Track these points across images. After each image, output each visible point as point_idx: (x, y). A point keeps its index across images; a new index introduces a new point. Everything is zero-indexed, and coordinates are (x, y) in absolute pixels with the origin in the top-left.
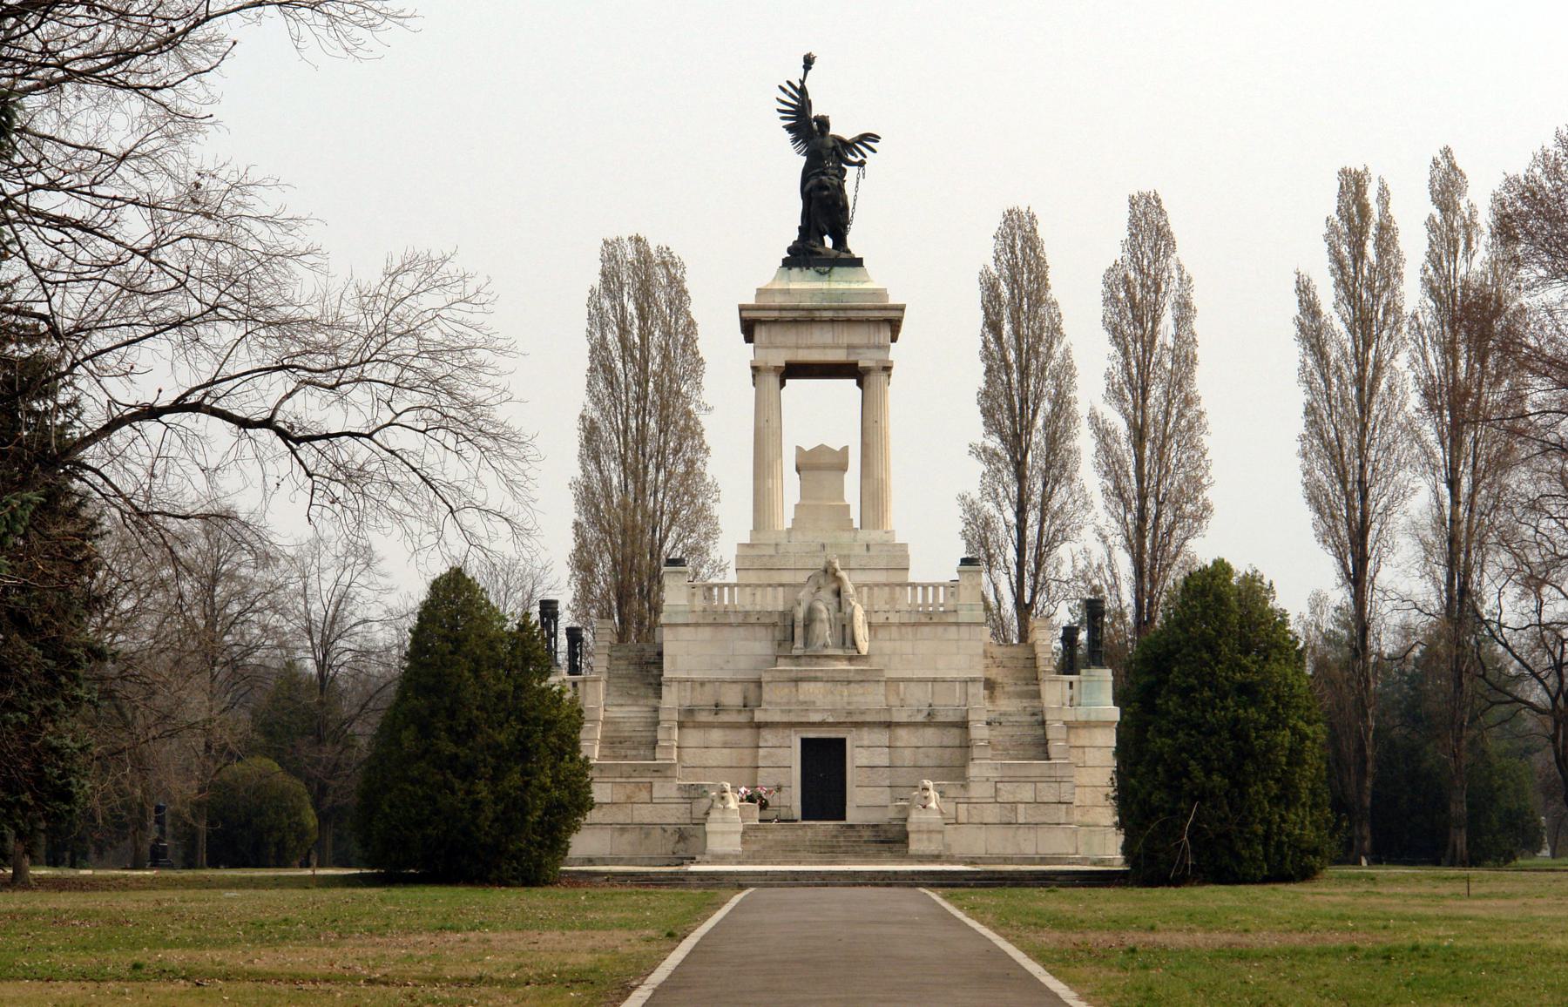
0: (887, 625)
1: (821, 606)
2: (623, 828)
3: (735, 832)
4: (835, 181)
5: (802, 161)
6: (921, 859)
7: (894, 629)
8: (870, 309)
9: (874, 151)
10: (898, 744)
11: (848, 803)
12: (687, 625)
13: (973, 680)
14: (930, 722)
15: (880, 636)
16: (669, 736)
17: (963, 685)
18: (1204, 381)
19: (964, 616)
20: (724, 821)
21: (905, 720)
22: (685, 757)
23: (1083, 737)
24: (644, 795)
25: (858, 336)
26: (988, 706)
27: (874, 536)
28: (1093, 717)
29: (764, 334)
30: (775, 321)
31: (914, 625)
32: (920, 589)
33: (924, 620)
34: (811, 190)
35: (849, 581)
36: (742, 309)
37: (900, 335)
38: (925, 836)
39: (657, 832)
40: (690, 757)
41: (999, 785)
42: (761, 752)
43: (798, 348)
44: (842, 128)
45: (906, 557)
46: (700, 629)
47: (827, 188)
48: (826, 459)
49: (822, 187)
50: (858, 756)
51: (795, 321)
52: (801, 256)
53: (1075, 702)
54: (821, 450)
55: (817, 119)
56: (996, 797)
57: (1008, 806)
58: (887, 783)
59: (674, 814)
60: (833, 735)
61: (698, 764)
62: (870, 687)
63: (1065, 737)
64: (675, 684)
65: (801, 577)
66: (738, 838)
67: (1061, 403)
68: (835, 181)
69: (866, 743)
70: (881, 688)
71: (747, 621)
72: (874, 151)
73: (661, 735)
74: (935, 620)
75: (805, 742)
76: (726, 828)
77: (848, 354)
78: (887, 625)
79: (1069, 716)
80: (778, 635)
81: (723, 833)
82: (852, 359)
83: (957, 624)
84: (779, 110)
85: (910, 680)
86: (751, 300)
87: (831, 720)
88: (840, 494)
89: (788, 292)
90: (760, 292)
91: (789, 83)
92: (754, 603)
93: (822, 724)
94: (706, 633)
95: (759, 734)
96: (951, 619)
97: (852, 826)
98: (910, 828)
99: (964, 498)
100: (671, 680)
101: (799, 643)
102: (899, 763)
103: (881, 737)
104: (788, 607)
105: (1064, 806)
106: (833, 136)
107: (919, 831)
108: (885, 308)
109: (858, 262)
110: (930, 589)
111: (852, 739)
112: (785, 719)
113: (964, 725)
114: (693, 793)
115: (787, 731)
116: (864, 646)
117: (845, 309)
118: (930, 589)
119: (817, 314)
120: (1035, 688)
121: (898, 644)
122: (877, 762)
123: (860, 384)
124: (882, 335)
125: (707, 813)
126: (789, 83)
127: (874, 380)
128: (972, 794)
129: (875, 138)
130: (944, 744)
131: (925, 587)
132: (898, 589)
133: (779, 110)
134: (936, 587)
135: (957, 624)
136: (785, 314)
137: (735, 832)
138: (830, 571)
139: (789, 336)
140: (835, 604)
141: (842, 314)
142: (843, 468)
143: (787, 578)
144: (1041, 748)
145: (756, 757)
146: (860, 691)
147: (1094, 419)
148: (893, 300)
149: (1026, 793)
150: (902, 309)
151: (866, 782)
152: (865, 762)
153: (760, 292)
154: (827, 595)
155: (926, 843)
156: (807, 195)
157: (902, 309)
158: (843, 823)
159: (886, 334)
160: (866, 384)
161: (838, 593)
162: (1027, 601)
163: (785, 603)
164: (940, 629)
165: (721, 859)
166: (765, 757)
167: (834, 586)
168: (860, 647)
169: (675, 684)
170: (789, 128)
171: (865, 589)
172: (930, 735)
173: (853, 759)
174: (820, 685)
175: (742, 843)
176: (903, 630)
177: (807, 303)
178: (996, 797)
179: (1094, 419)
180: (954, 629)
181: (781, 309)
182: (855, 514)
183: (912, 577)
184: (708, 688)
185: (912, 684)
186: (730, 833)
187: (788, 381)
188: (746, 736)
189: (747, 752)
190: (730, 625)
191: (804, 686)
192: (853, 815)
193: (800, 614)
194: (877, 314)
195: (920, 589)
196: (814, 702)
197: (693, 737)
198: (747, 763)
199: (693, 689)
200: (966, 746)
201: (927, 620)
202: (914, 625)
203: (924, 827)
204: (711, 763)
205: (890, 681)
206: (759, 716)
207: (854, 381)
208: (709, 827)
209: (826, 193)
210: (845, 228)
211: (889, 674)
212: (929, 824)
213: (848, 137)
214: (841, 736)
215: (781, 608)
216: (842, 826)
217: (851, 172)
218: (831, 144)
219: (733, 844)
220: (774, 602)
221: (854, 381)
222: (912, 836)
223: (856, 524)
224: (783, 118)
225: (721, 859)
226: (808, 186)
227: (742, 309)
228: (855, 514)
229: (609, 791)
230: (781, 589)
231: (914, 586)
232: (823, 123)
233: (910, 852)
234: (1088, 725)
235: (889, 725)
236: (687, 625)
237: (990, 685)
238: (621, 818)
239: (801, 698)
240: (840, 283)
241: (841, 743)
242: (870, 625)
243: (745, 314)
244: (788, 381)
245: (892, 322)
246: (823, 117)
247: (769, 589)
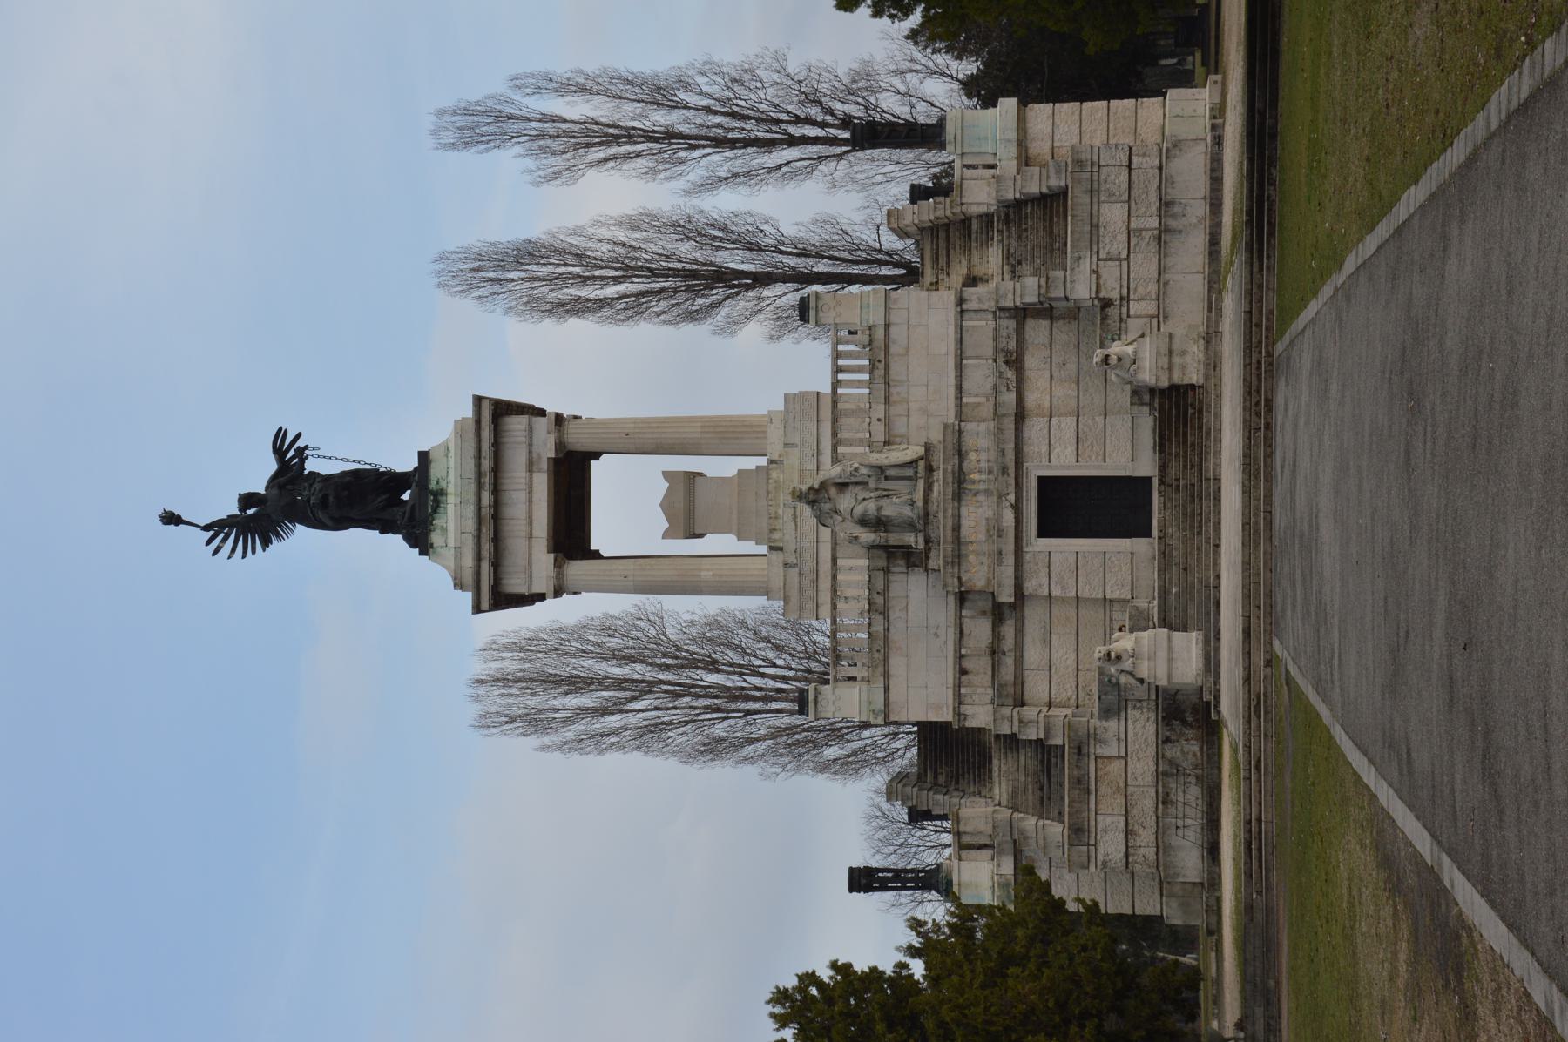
0: (887, 422)
1: (859, 510)
2: (1165, 800)
3: (1169, 639)
4: (317, 486)
5: (300, 530)
6: (1212, 365)
7: (893, 410)
8: (479, 441)
9: (299, 435)
10: (1047, 404)
11: (1128, 473)
12: (886, 689)
13: (961, 301)
14: (1015, 361)
15: (903, 430)
16: (1031, 723)
17: (966, 316)
18: (655, 62)
19: (877, 317)
20: (1152, 657)
21: (1013, 395)
22: (1064, 696)
23: (1040, 148)
24: (1115, 768)
25: (516, 460)
26: (996, 279)
27: (775, 436)
28: (1013, 135)
29: (513, 581)
30: (496, 565)
31: (887, 384)
32: (840, 376)
33: (880, 372)
34: (332, 518)
35: (832, 471)
36: (477, 609)
37: (538, 405)
38: (1177, 360)
39: (1172, 752)
40: (1064, 691)
41: (1103, 255)
42: (1056, 592)
43: (530, 537)
44: (258, 473)
45: (802, 396)
46: (892, 671)
47: (325, 497)
48: (680, 503)
49: (324, 502)
50: (1064, 463)
51: (497, 539)
52: (420, 540)
53: (991, 161)
54: (667, 506)
55: (243, 508)
56: (1120, 260)
57: (1134, 241)
58: (1100, 419)
59: (1142, 727)
60: (1033, 494)
61: (1072, 681)
62: (969, 442)
63: (1038, 169)
64: (963, 709)
65: (826, 533)
66: (1178, 636)
67: (685, 229)
68: (317, 486)
69: (1044, 449)
70: (969, 427)
71: (879, 607)
72: (299, 435)
73: (1031, 734)
74: (882, 357)
75: (1043, 533)
76: (1162, 654)
77: (540, 471)
78: (887, 422)
79: (1008, 165)
80: (899, 567)
81: (1170, 660)
82: (545, 466)
83: (887, 326)
84: (244, 557)
85: (959, 388)
86: (467, 597)
87: (1012, 497)
88: (723, 481)
89: (458, 550)
90: (459, 585)
91: (209, 542)
92: (858, 599)
93: (1017, 508)
94: (897, 664)
95: (1031, 596)
96: (880, 333)
97: (1162, 468)
98: (1165, 383)
99: (771, 337)
100: (957, 712)
101: (910, 538)
102: (1074, 403)
103: (1035, 429)
104: (864, 551)
105: (1135, 159)
106: (267, 488)
107: (1170, 369)
108: (478, 422)
109: (424, 457)
110: (840, 362)
111: (1037, 468)
112: (1010, 560)
113: (1021, 314)
114: (1115, 699)
115: (1028, 557)
116: (914, 451)
117: (479, 475)
118: (840, 362)
119: (485, 511)
120: (974, 222)
121: (913, 406)
122: (1070, 434)
123: (596, 455)
124: (512, 427)
125: (1141, 681)
126: (209, 542)
127: (578, 439)
128: (1115, 295)
129: (281, 434)
130: (1047, 341)
131: (837, 370)
132: (840, 406)
133: (244, 557)
134: (837, 355)
135: (887, 326)
136: (485, 553)
137: (1169, 639)
138: (811, 497)
139: (516, 546)
140: (857, 489)
141: (486, 480)
142: (691, 478)
143: (826, 554)
144: (1052, 203)
145: (1063, 600)
146: (972, 456)
147: (688, 193)
148: (468, 411)
149: (1113, 214)
150: (478, 400)
151: (1098, 448)
152: (1071, 450)
153: (459, 585)
154: (845, 502)
155: (1188, 358)
156: (339, 523)
157: (478, 400)
158: (1155, 482)
159: (516, 425)
160: (598, 449)
161: (842, 486)
162: (903, 271)
163: (858, 557)
164: (893, 349)
165: (1211, 663)
166: (1063, 588)
167: (833, 491)
168: (915, 456)
169: (963, 709)
170: (266, 543)
171: (840, 449)
172: (1032, 362)
173: (1068, 467)
174: (964, 511)
175: (1185, 630)
176: (893, 398)
177: (470, 525)
178: (1120, 260)
179: (688, 193)
180: (893, 330)
181: (478, 558)
182: (750, 463)
183: (826, 389)
184: (967, 664)
185: (965, 385)
186: (1170, 649)
187: (593, 547)
188: (1034, 617)
189: (1055, 611)
190: (887, 630)
191: (966, 532)
192: (1146, 466)
193: (867, 536)
194: (486, 434)
195: (840, 376)
196: (987, 519)
197: (1036, 688)
198: (1073, 613)
199: (970, 684)
200: (1045, 310)
201: (881, 366)
202: (887, 384)
203: (1164, 361)
204: (1071, 661)
205: (960, 415)
206: (1007, 596)
207: (593, 463)
208: (1163, 682)
209: (331, 499)
210: (383, 473)
211: (951, 419)
212: (1158, 353)
213: (272, 466)
214: (1034, 483)
215: (865, 562)
216: (1161, 482)
217: (311, 466)
218: (275, 491)
219: (1189, 646)
220: (855, 571)
221: (593, 463)
222: (1177, 379)
223: (763, 461)
224: (254, 551)
225: (1211, 663)
226: (329, 523)
227: (477, 609)
228: (750, 463)
229: (1109, 820)
230: (840, 562)
231: (836, 384)
232: (247, 500)
233: (1201, 382)
234: (1022, 143)
235: (1020, 416)
236: (886, 689)
237: (972, 281)
238: (1146, 803)
239: (982, 537)
240: (452, 476)
241: (1047, 485)
242: (887, 443)
243: (485, 605)
244: (593, 547)
245: (499, 412)
246: (239, 500)
247: (839, 577)
